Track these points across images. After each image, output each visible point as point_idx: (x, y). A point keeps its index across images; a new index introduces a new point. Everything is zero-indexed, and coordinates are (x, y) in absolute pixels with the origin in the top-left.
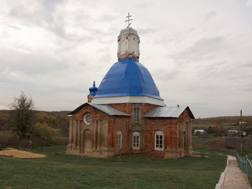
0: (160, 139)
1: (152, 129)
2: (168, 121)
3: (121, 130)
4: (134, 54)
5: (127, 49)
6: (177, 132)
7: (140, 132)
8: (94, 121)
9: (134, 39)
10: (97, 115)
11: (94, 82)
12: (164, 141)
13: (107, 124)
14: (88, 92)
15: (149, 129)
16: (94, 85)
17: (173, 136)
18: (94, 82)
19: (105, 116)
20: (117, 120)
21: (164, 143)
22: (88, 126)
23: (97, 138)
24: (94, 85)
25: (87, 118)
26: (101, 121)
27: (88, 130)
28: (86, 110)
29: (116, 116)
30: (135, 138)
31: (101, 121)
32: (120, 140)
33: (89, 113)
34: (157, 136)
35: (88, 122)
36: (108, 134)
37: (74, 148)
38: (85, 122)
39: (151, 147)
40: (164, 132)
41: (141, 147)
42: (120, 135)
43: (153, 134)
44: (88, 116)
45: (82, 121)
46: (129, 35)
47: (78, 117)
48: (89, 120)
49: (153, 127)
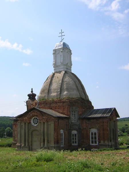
0: (93, 141)
1: (88, 127)
2: (101, 120)
3: (63, 129)
4: (68, 64)
5: (62, 61)
6: (108, 129)
7: (77, 131)
8: (41, 122)
9: (67, 52)
10: (44, 117)
11: (32, 89)
12: (98, 136)
13: (53, 124)
14: (27, 98)
15: (85, 127)
16: (32, 92)
17: (105, 132)
18: (32, 89)
19: (51, 118)
20: (60, 121)
21: (98, 139)
22: (35, 128)
23: (44, 136)
24: (32, 92)
25: (34, 120)
26: (47, 122)
27: (35, 130)
28: (33, 114)
29: (59, 118)
30: (73, 136)
31: (47, 122)
32: (62, 138)
33: (37, 116)
34: (92, 134)
35: (35, 124)
36: (54, 133)
37: (23, 147)
38: (32, 123)
39: (87, 142)
40: (98, 130)
41: (78, 143)
42: (62, 134)
43: (89, 132)
44: (35, 118)
45: (30, 123)
46: (64, 53)
47: (25, 120)
48: (36, 121)
49: (88, 126)
